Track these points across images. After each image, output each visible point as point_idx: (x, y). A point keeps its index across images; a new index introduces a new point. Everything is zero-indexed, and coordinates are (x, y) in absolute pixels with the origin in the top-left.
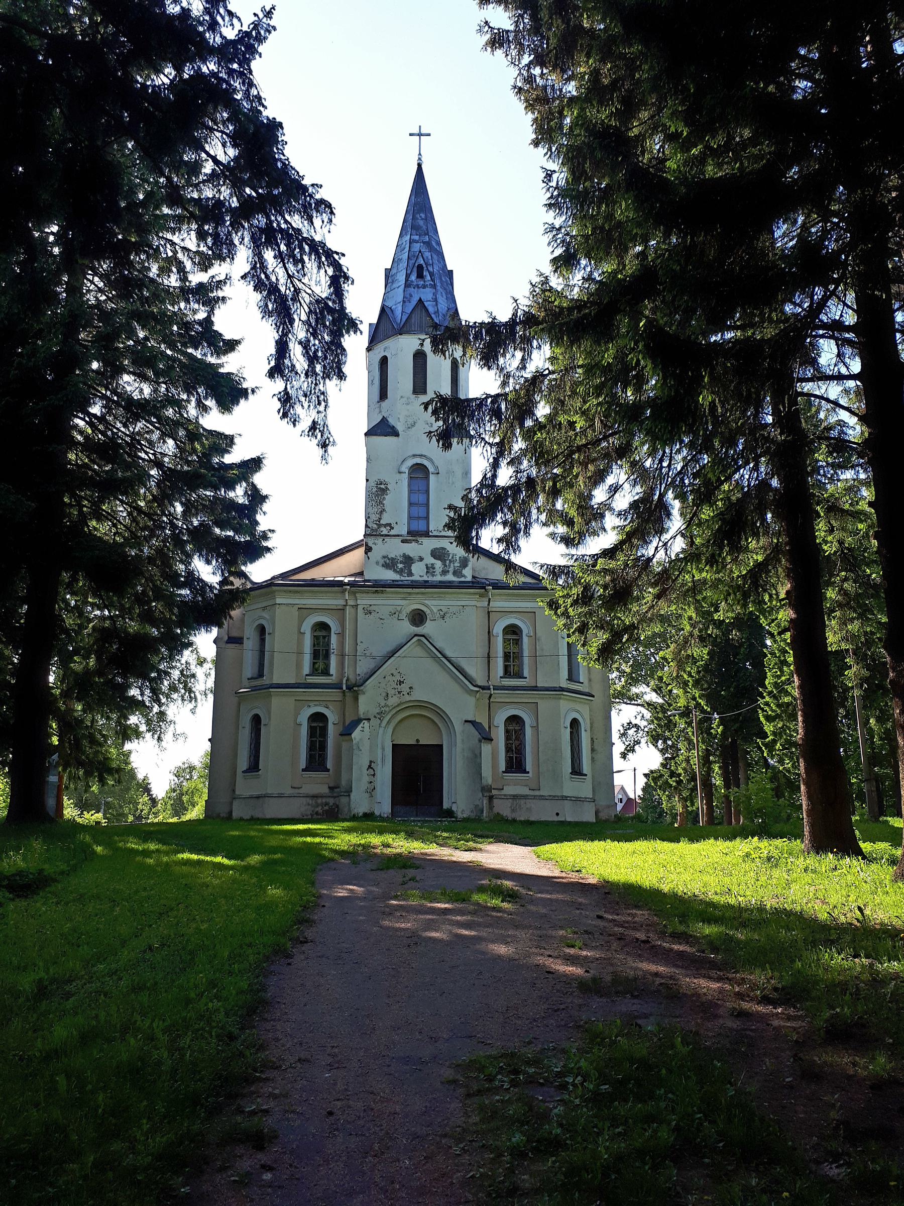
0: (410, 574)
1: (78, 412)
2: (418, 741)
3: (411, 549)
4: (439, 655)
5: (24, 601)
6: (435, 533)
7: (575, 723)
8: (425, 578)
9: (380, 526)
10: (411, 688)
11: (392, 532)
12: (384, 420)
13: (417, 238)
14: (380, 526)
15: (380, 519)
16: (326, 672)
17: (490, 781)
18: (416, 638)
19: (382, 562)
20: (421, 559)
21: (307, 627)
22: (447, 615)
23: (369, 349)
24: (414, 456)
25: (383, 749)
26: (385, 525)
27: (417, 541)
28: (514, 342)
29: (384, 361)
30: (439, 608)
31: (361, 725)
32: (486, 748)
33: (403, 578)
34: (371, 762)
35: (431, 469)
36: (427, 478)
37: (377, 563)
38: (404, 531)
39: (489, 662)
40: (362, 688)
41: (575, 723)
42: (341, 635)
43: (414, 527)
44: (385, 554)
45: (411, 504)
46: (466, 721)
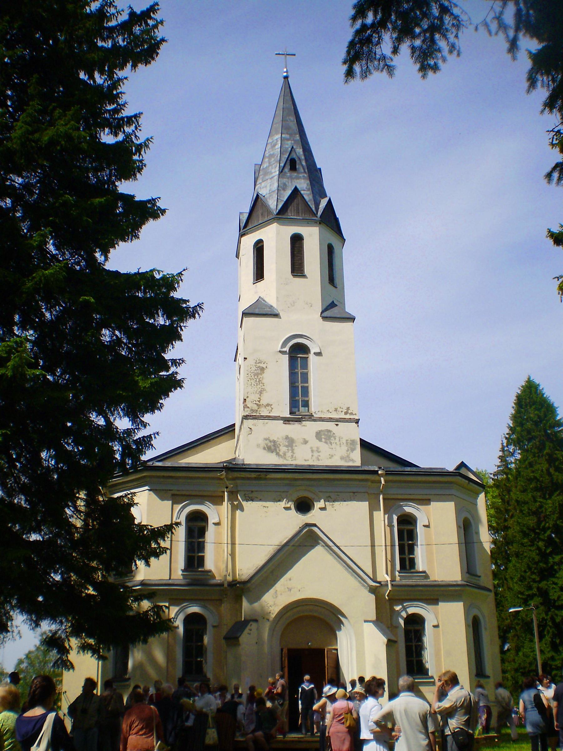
1: (131, 459)
3: (294, 430)
5: (38, 186)
7: (259, 274)
13: (288, 136)
19: (263, 444)
20: (306, 442)
28: (148, 32)
31: (249, 627)
37: (258, 446)
41: (259, 274)
44: (266, 437)
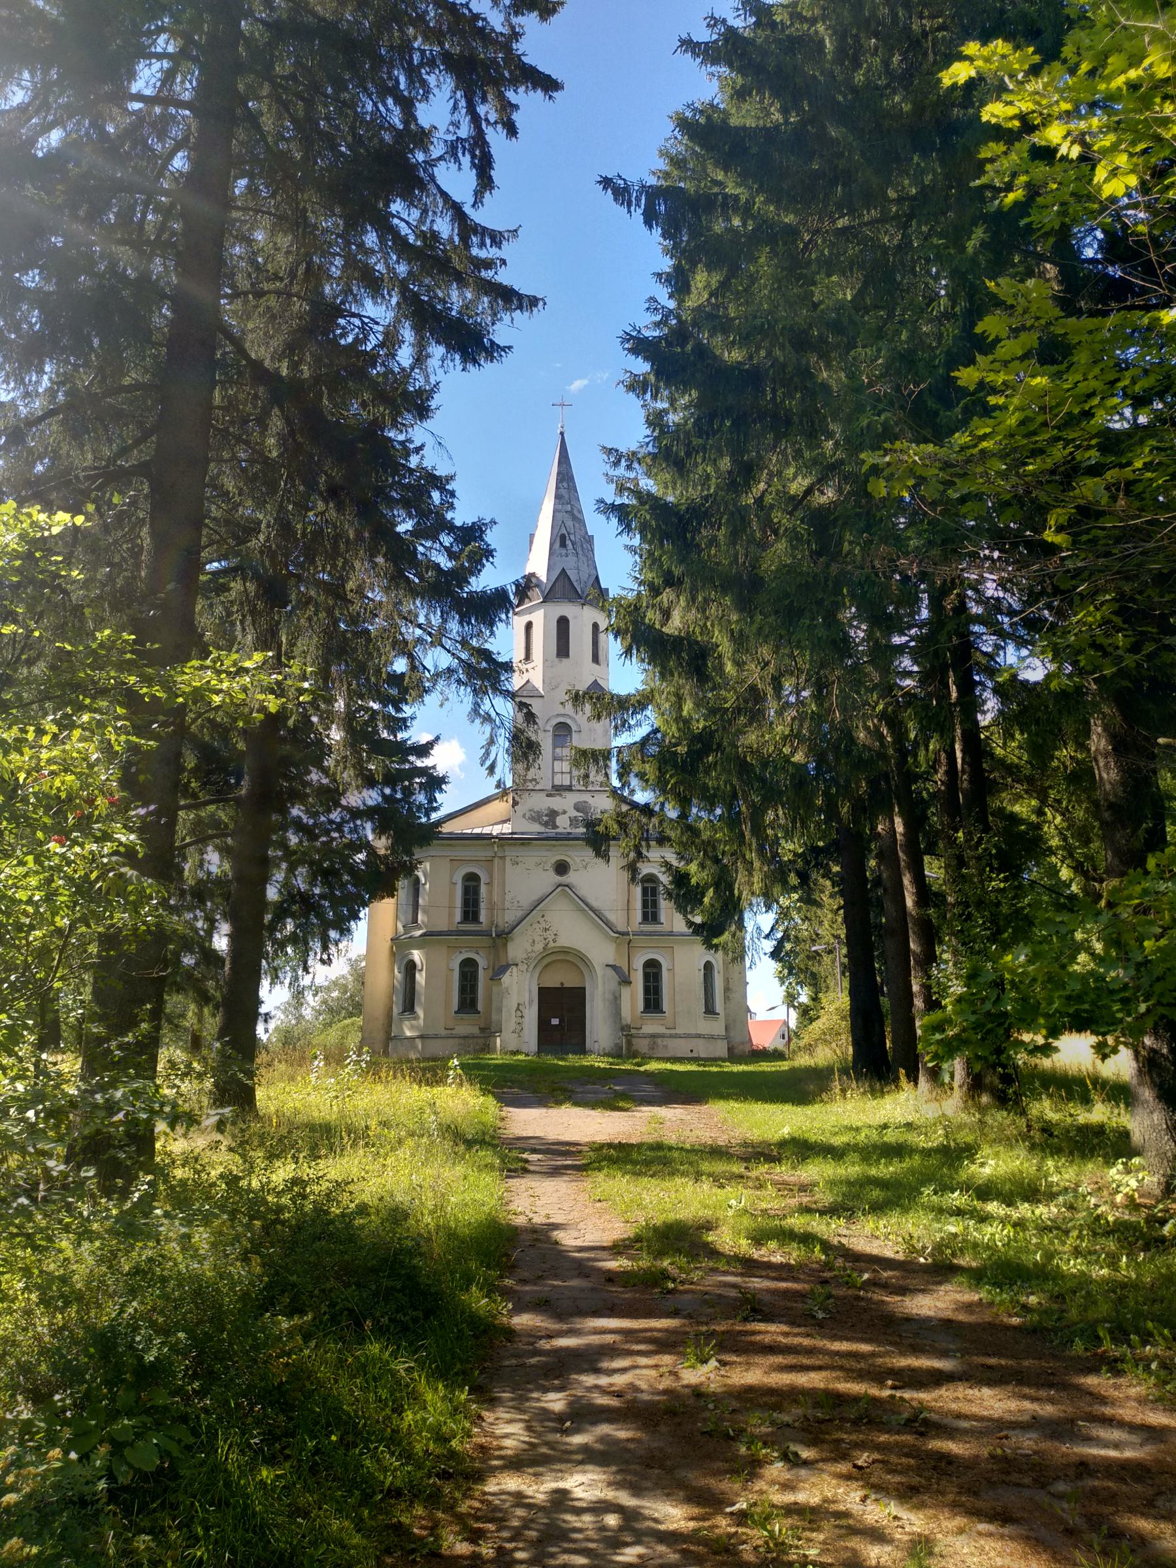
0: (555, 827)
17: (629, 1021)
32: (626, 993)
35: (574, 728)
43: (557, 782)
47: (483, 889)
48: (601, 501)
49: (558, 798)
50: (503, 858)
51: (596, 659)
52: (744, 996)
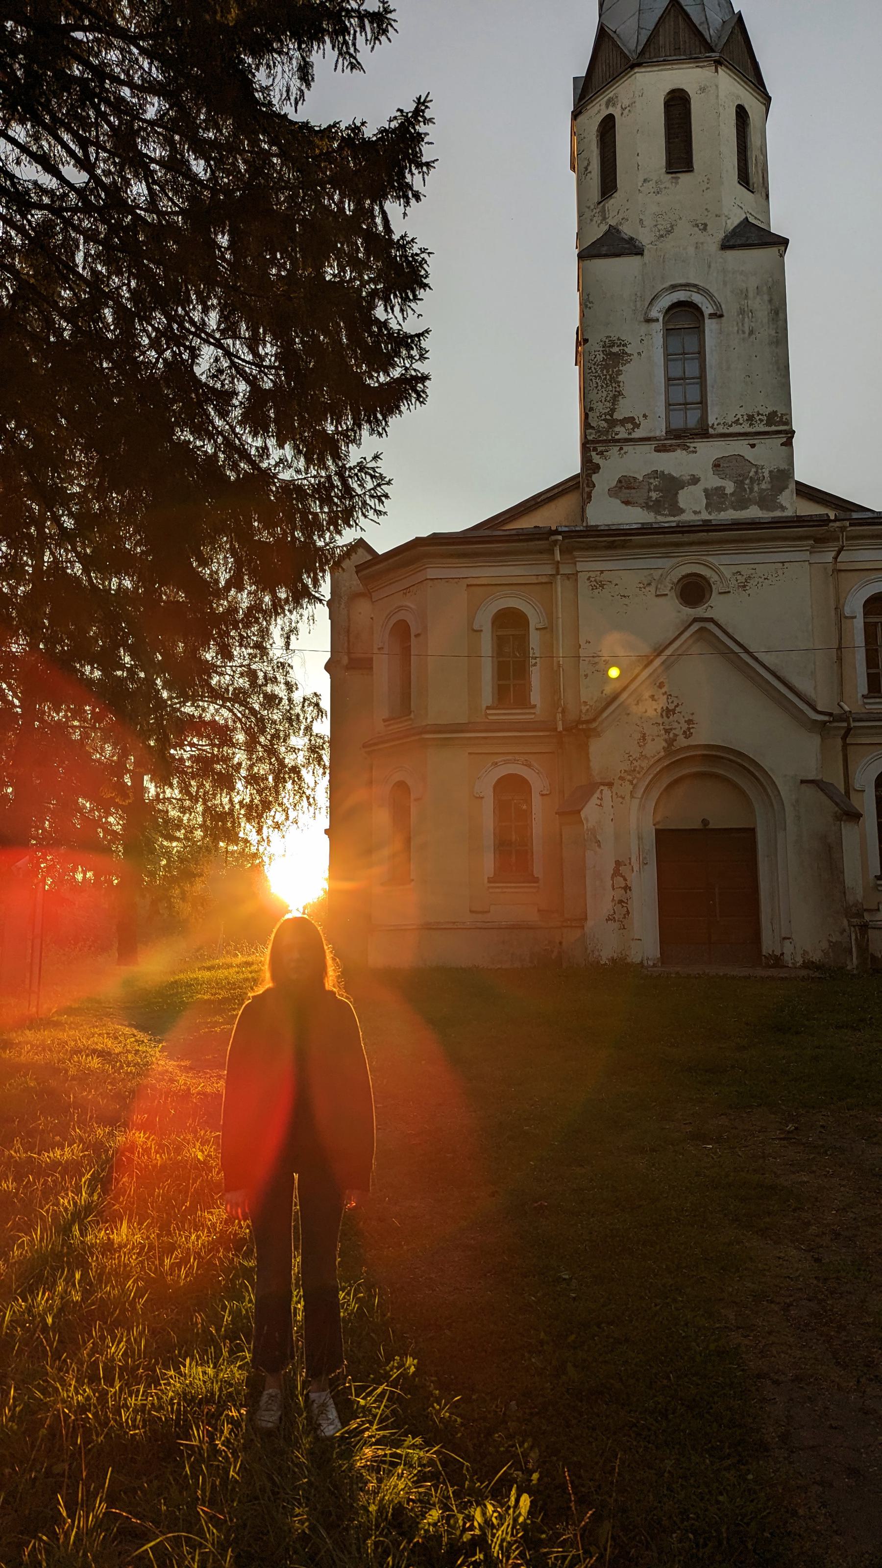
0: (677, 510)
2: (705, 822)
4: (737, 649)
6: (721, 430)
8: (705, 516)
9: (612, 423)
10: (689, 722)
11: (638, 434)
12: (613, 233)
14: (612, 423)
15: (613, 410)
16: (523, 701)
17: (859, 895)
18: (695, 627)
21: (484, 619)
22: (753, 582)
23: (575, 115)
24: (674, 288)
25: (640, 838)
26: (624, 422)
27: (685, 448)
29: (608, 126)
30: (735, 569)
31: (597, 794)
32: (850, 833)
33: (660, 518)
34: (618, 863)
35: (707, 309)
36: (699, 330)
38: (660, 431)
39: (840, 659)
40: (594, 725)
42: (548, 629)
43: (678, 423)
45: (669, 380)
46: (802, 782)
47: (535, 640)
48: (430, 379)
49: (679, 454)
50: (573, 577)
51: (744, 178)
52: (321, 905)
